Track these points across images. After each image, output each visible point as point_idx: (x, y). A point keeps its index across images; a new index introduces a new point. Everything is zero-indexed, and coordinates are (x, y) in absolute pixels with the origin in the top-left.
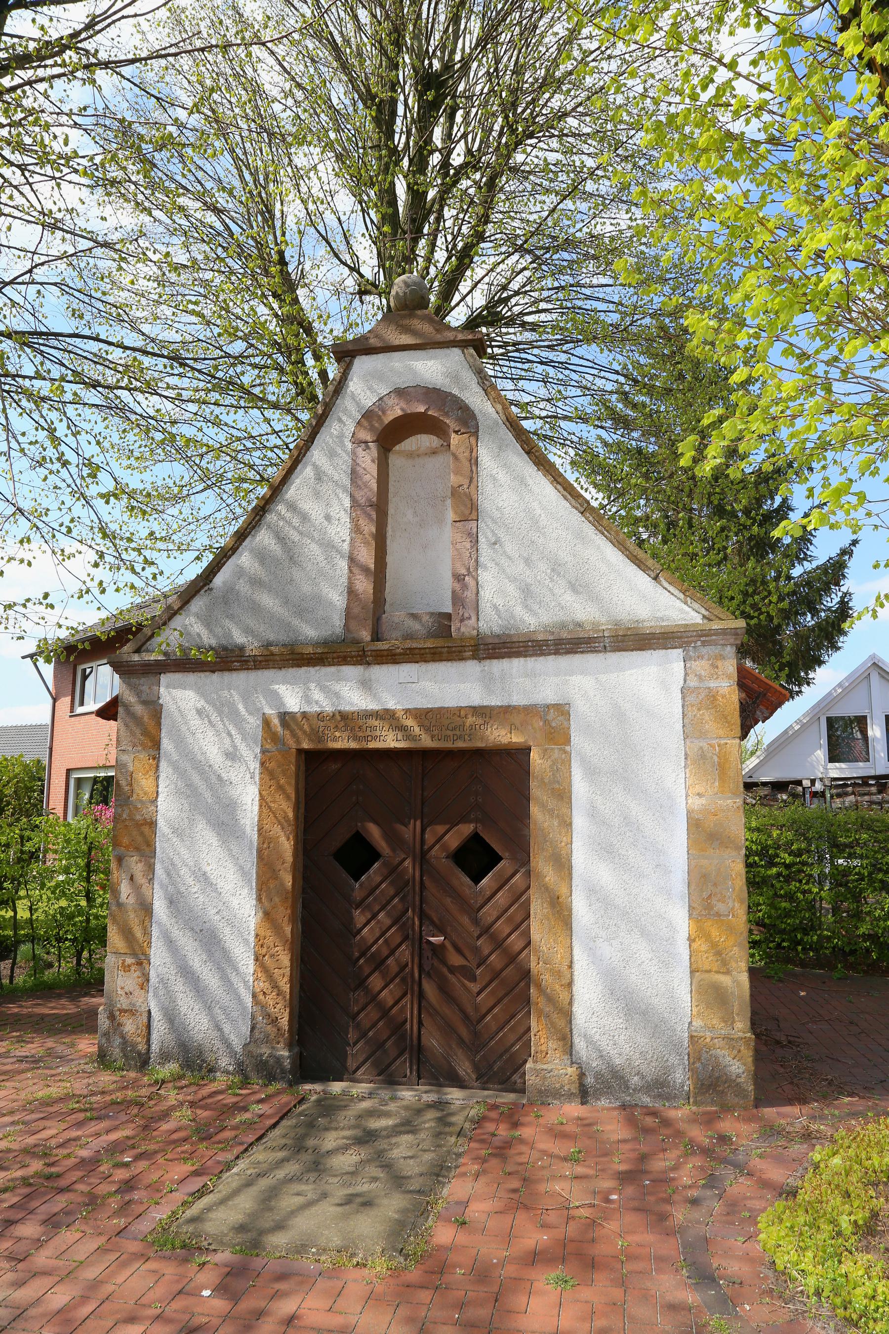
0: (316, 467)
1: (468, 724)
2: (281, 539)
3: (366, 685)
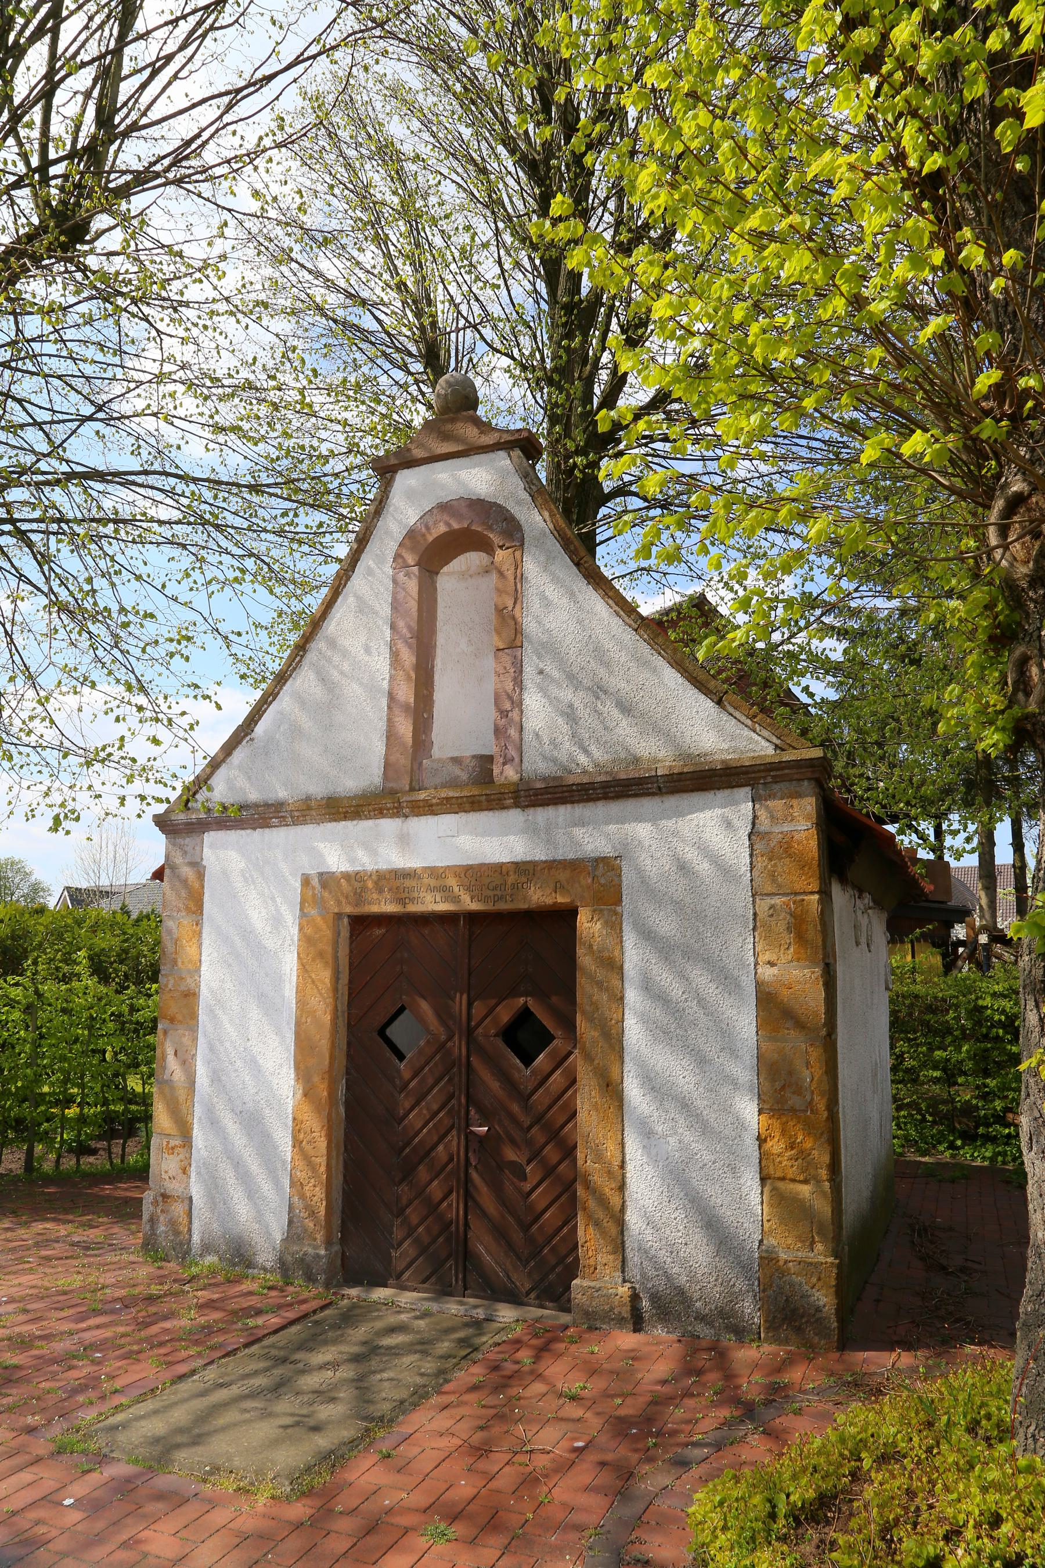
0: (358, 598)
1: (509, 882)
2: (323, 679)
3: (404, 841)
